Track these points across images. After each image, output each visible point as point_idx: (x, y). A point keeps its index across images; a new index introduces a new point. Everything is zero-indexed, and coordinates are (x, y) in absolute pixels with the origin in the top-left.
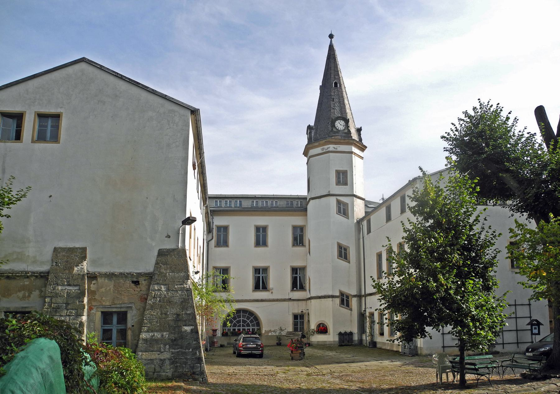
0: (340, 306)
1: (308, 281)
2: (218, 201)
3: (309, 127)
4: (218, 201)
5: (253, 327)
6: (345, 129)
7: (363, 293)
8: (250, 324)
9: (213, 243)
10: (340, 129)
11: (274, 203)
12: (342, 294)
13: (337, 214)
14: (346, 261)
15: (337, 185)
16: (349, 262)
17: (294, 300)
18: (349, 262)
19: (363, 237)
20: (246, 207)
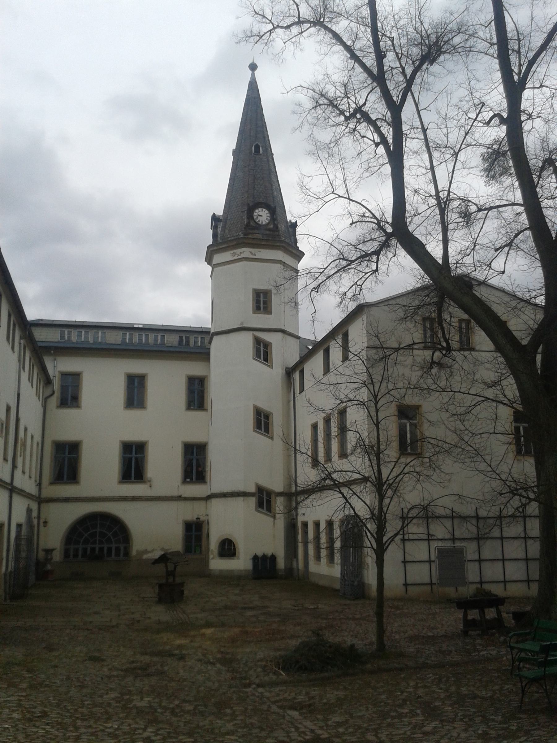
0: (256, 510)
1: (209, 464)
2: (83, 332)
3: (215, 218)
4: (83, 332)
5: (92, 546)
6: (268, 224)
7: (293, 489)
8: (113, 540)
9: (54, 401)
10: (260, 223)
11: (159, 337)
12: (260, 490)
13: (254, 359)
14: (267, 436)
15: (254, 312)
16: (272, 438)
17: (186, 499)
18: (272, 438)
19: (294, 398)
20: (114, 342)
